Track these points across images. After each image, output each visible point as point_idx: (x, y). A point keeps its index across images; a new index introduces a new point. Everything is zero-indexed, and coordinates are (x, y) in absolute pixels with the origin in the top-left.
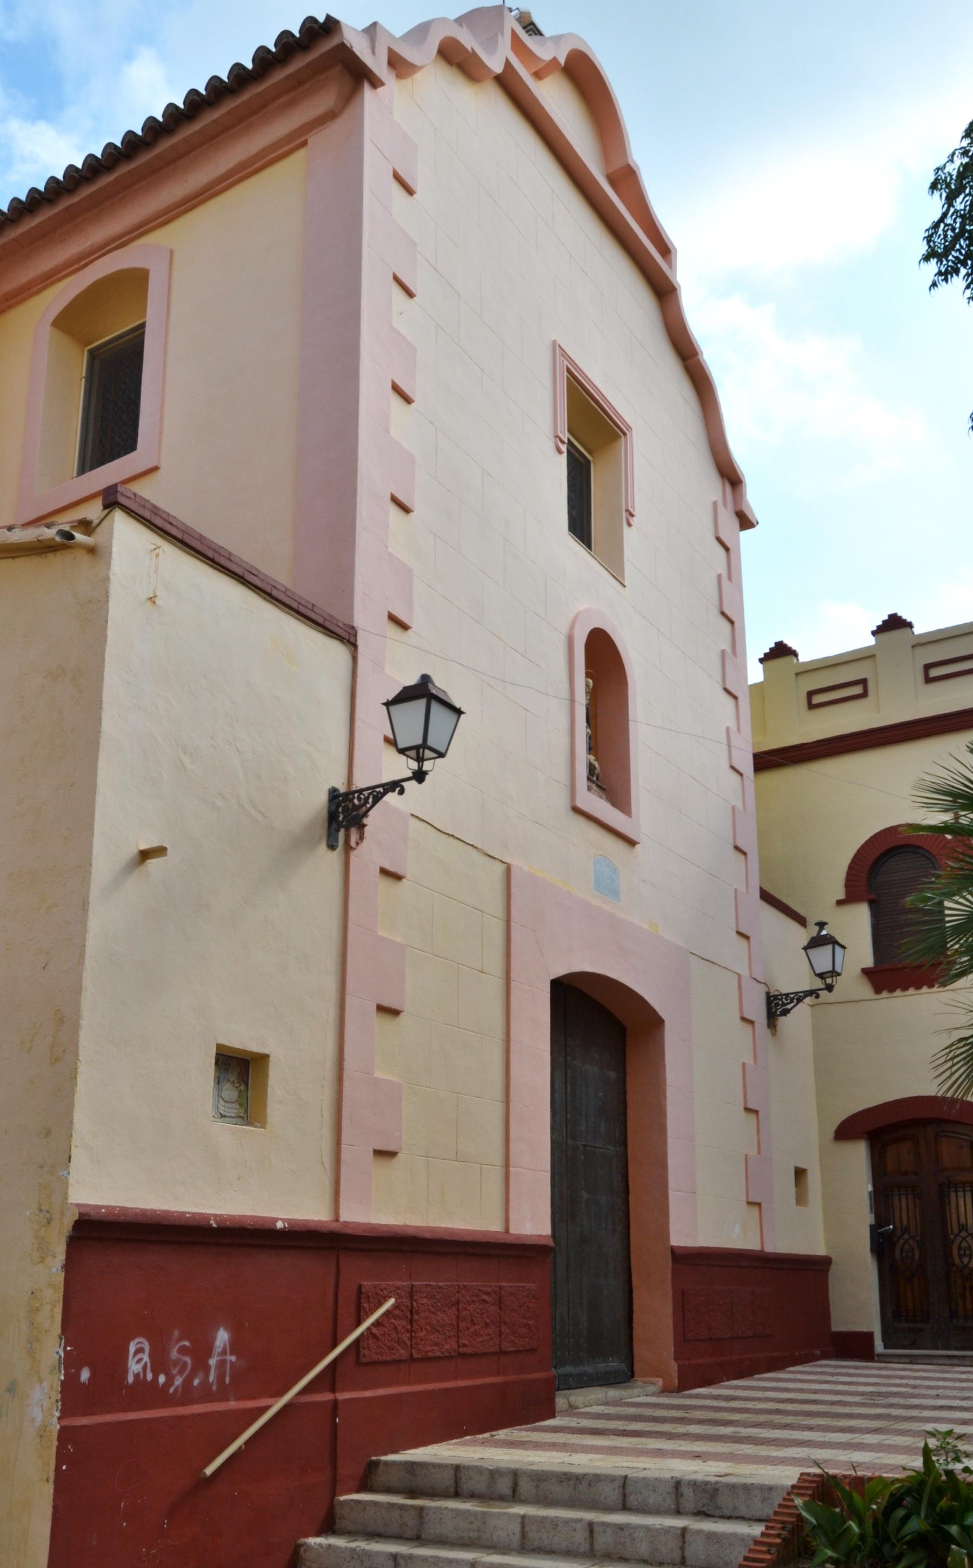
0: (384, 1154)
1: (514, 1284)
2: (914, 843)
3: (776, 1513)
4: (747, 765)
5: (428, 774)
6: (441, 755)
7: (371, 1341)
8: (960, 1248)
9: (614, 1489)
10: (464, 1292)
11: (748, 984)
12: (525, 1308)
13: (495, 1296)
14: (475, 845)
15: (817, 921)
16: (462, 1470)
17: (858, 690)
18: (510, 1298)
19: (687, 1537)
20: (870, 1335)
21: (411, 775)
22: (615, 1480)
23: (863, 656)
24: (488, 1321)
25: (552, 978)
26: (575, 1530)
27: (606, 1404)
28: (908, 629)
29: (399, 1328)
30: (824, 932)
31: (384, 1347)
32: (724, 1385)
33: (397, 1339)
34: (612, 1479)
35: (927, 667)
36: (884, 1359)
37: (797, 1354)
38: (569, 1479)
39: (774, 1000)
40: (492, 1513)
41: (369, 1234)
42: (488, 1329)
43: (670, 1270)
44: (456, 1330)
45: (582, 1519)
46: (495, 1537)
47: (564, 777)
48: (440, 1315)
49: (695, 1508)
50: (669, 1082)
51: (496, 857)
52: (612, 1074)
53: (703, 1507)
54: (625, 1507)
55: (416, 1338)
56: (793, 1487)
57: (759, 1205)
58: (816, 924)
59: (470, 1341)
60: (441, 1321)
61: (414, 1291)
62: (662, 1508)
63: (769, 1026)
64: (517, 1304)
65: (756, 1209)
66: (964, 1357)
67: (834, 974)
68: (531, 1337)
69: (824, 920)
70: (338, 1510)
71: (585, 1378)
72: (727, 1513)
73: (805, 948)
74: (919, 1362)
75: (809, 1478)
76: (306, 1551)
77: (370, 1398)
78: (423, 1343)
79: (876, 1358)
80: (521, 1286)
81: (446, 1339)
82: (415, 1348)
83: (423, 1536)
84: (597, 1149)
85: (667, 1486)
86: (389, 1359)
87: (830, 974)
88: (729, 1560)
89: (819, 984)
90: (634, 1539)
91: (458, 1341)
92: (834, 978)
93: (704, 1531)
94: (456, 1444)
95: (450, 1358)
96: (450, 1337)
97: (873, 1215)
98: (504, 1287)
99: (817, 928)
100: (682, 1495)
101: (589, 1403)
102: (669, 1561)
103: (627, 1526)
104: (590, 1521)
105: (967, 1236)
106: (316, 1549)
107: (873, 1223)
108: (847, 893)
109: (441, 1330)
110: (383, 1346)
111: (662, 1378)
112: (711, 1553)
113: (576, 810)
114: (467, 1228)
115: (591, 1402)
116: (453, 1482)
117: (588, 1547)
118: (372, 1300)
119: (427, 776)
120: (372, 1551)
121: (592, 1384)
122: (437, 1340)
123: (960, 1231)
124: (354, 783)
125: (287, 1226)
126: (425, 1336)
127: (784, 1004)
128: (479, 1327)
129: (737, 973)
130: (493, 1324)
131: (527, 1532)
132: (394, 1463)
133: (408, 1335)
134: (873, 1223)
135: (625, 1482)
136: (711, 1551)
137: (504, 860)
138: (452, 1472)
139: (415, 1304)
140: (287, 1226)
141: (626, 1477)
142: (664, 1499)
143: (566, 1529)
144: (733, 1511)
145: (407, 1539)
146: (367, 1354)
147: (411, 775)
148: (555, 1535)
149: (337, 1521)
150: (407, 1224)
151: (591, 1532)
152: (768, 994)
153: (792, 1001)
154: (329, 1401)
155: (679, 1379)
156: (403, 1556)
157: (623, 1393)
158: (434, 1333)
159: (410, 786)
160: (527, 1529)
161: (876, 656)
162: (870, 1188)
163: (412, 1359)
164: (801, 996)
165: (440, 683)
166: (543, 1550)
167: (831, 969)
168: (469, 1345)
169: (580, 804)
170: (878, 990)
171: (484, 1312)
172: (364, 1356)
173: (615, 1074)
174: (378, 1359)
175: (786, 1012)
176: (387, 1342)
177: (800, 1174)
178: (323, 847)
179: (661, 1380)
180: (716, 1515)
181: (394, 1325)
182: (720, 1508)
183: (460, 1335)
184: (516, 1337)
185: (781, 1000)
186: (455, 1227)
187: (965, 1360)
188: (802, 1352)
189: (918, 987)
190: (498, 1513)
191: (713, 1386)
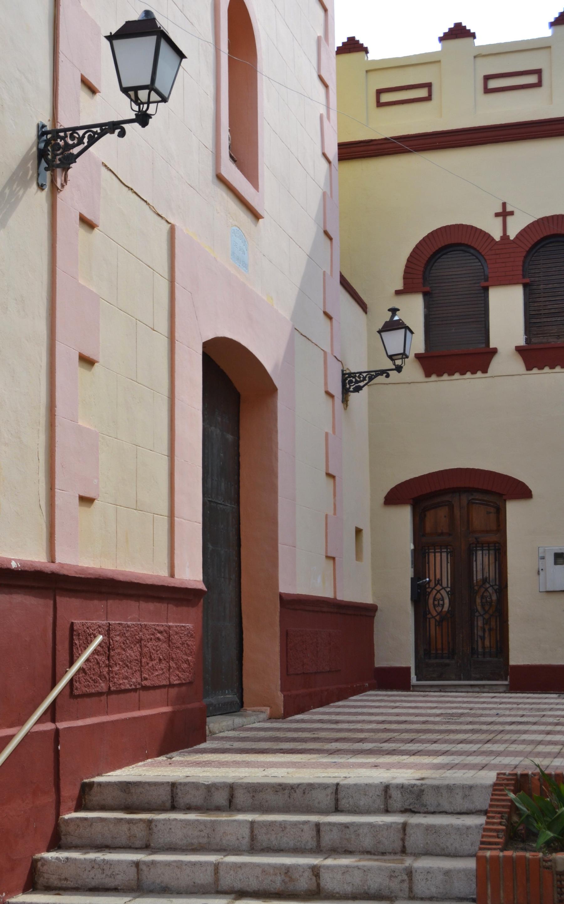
0: (86, 501)
1: (179, 624)
2: (466, 243)
3: (491, 806)
4: (333, 152)
5: (151, 118)
6: (164, 100)
7: (81, 675)
8: (435, 599)
9: (327, 795)
10: (144, 630)
11: (331, 359)
12: (186, 645)
13: (165, 635)
14: (148, 201)
15: (390, 307)
16: (179, 787)
17: (532, 79)
18: (176, 636)
19: (408, 830)
20: (408, 669)
21: (134, 117)
22: (328, 787)
23: (413, 63)
24: (161, 657)
25: (204, 341)
26: (302, 831)
27: (234, 729)
28: (363, 53)
29: (101, 663)
30: (396, 318)
31: (90, 681)
32: (316, 712)
33: (99, 673)
34: (324, 787)
35: (379, 92)
36: (418, 689)
37: (355, 686)
38: (284, 789)
39: (349, 377)
40: (221, 821)
41: (80, 576)
42: (161, 665)
43: (278, 614)
44: (140, 665)
45: (309, 821)
46: (224, 842)
47: (209, 142)
48: (129, 651)
49: (403, 807)
50: (280, 446)
51: (163, 216)
52: (230, 437)
53: (409, 805)
54: (337, 810)
55: (112, 672)
56: (495, 784)
57: (334, 559)
58: (389, 310)
59: (149, 675)
60: (129, 657)
61: (110, 629)
62: (372, 809)
63: (343, 402)
64: (181, 642)
65: (331, 562)
66: (483, 686)
67: (404, 356)
68: (190, 671)
69: (397, 307)
70: (63, 828)
71: (211, 708)
72: (432, 809)
73: (380, 332)
74: (447, 690)
75: (505, 777)
76: (43, 865)
77: (81, 727)
78: (117, 676)
79: (411, 689)
80: (183, 626)
81: (133, 674)
82: (112, 681)
83: (152, 845)
84: (218, 505)
85: (377, 790)
86: (93, 691)
87: (400, 356)
88: (445, 847)
89: (388, 364)
90: (359, 835)
91: (141, 675)
92: (403, 360)
93: (422, 824)
94: (144, 765)
95: (135, 690)
96: (135, 671)
97: (413, 569)
98: (172, 626)
99: (390, 314)
100: (390, 797)
101: (222, 729)
102: (390, 851)
103: (352, 824)
104: (316, 822)
105: (441, 589)
106: (54, 862)
107: (413, 577)
108: (405, 284)
109: (129, 665)
110: (89, 679)
111: (269, 707)
112: (429, 842)
113: (220, 179)
114: (144, 573)
115: (224, 727)
116: (169, 797)
117: (315, 844)
118: (81, 637)
119: (150, 120)
120: (113, 861)
121: (215, 714)
122: (127, 674)
123: (436, 585)
124: (59, 120)
125: (19, 566)
126: (118, 670)
127: (357, 382)
128: (155, 662)
129: (324, 351)
130: (165, 659)
131: (256, 835)
132: (109, 784)
133: (107, 669)
134: (413, 577)
135: (337, 789)
136: (429, 840)
137: (169, 221)
138: (169, 788)
139: (111, 641)
140: (19, 566)
141: (338, 784)
142: (374, 802)
143: (294, 830)
144: (437, 806)
145: (136, 849)
146: (79, 687)
147: (134, 117)
148: (284, 836)
149: (63, 837)
150: (103, 567)
151: (318, 831)
152: (343, 371)
153: (364, 379)
154: (51, 730)
155: (284, 708)
156: (145, 863)
157: (244, 720)
158: (124, 667)
159: (393, 374)
160: (256, 832)
161: (441, 61)
162: (412, 547)
163: (110, 692)
164: (373, 375)
165: (162, 22)
166: (271, 849)
167: (402, 351)
168: (149, 678)
169: (225, 173)
170: (428, 374)
171: (158, 649)
172: (77, 689)
173: (231, 437)
174: (86, 691)
175: (358, 389)
176: (92, 676)
177: (358, 531)
178: (35, 186)
179: (269, 708)
180: (421, 811)
181: (97, 660)
182: (425, 806)
183: (142, 670)
184: (180, 672)
185: (354, 377)
186: (136, 571)
187: (484, 688)
188: (358, 685)
189: (463, 373)
190: (227, 820)
191: (305, 713)
